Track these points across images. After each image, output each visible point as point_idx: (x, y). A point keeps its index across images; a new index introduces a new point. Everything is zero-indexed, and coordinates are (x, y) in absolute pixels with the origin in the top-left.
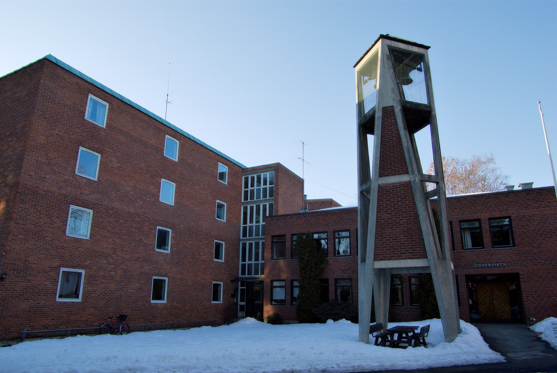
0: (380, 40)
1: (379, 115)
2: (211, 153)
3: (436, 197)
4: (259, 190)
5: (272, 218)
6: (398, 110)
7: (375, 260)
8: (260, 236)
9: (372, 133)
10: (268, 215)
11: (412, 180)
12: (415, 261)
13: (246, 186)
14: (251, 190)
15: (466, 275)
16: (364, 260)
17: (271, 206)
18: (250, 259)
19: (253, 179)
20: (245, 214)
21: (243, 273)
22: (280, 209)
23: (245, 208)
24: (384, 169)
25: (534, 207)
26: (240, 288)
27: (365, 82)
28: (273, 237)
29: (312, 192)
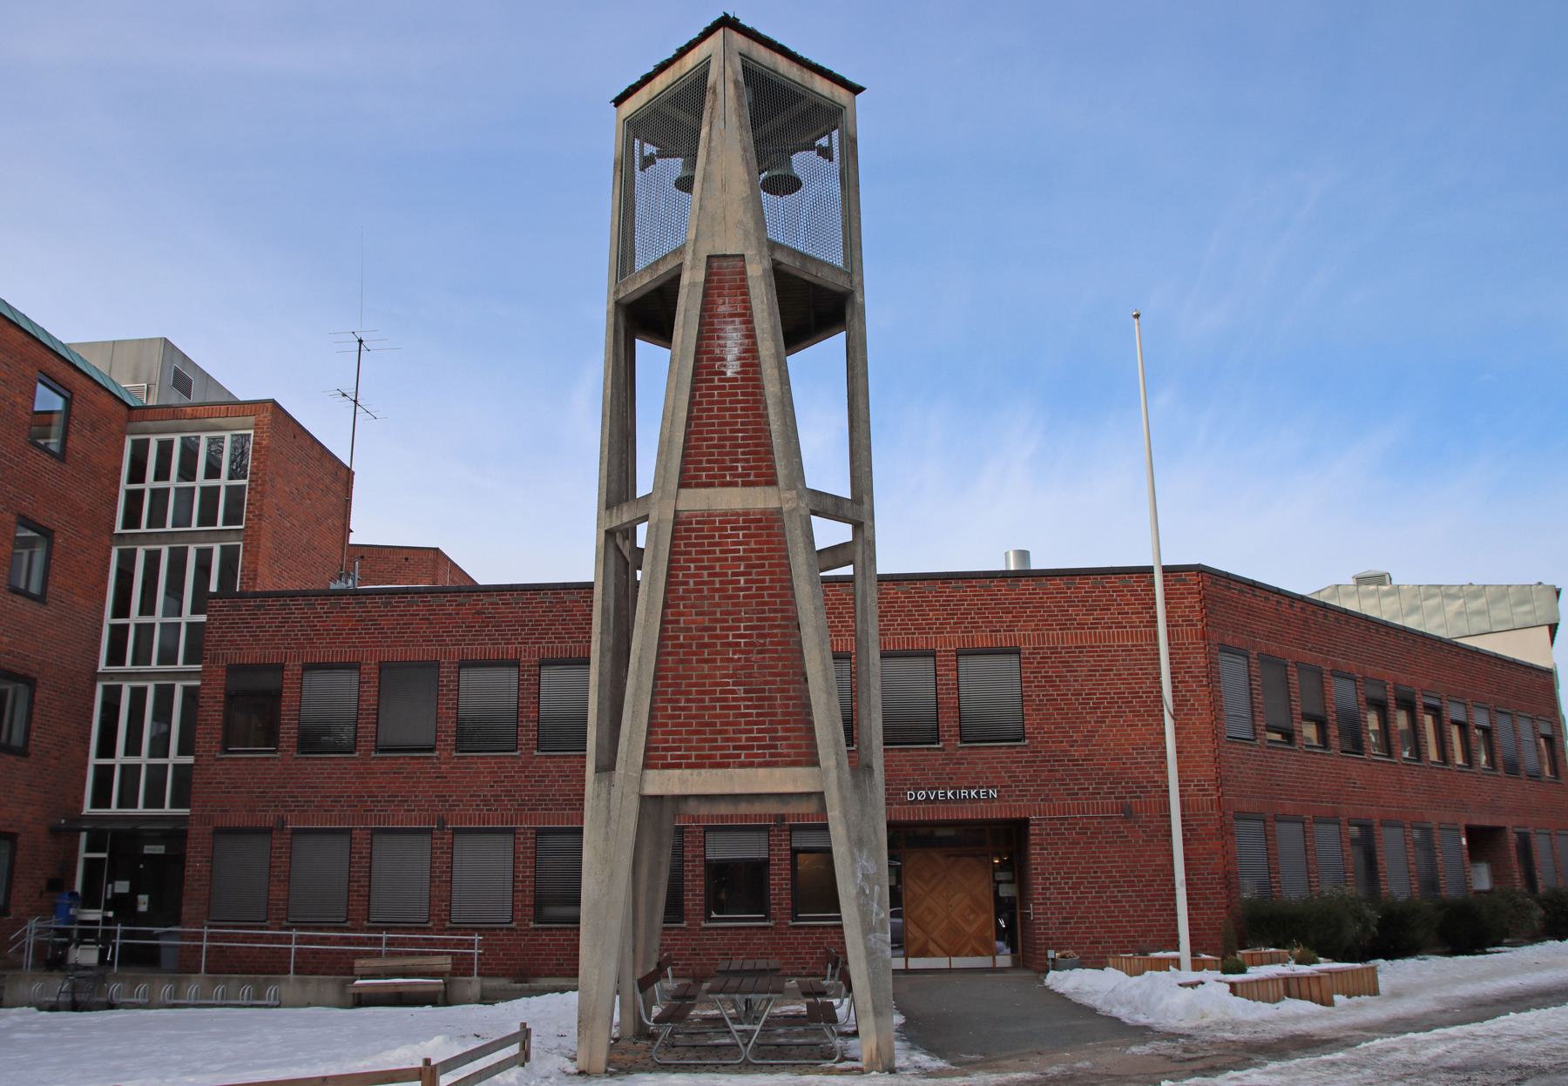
0: (721, 31)
1: (692, 279)
2: (12, 331)
3: (847, 570)
4: (185, 495)
5: (228, 597)
6: (757, 271)
7: (647, 765)
8: (180, 665)
9: (662, 332)
10: (213, 588)
11: (786, 507)
12: (778, 772)
13: (137, 474)
14: (154, 492)
15: (1024, 823)
16: (607, 766)
17: (229, 556)
18: (133, 748)
19: (165, 449)
20: (125, 577)
21: (101, 799)
22: (263, 569)
23: (127, 560)
24: (696, 462)
25: (1081, 626)
26: (83, 854)
27: (648, 161)
28: (233, 670)
29: (374, 522)
